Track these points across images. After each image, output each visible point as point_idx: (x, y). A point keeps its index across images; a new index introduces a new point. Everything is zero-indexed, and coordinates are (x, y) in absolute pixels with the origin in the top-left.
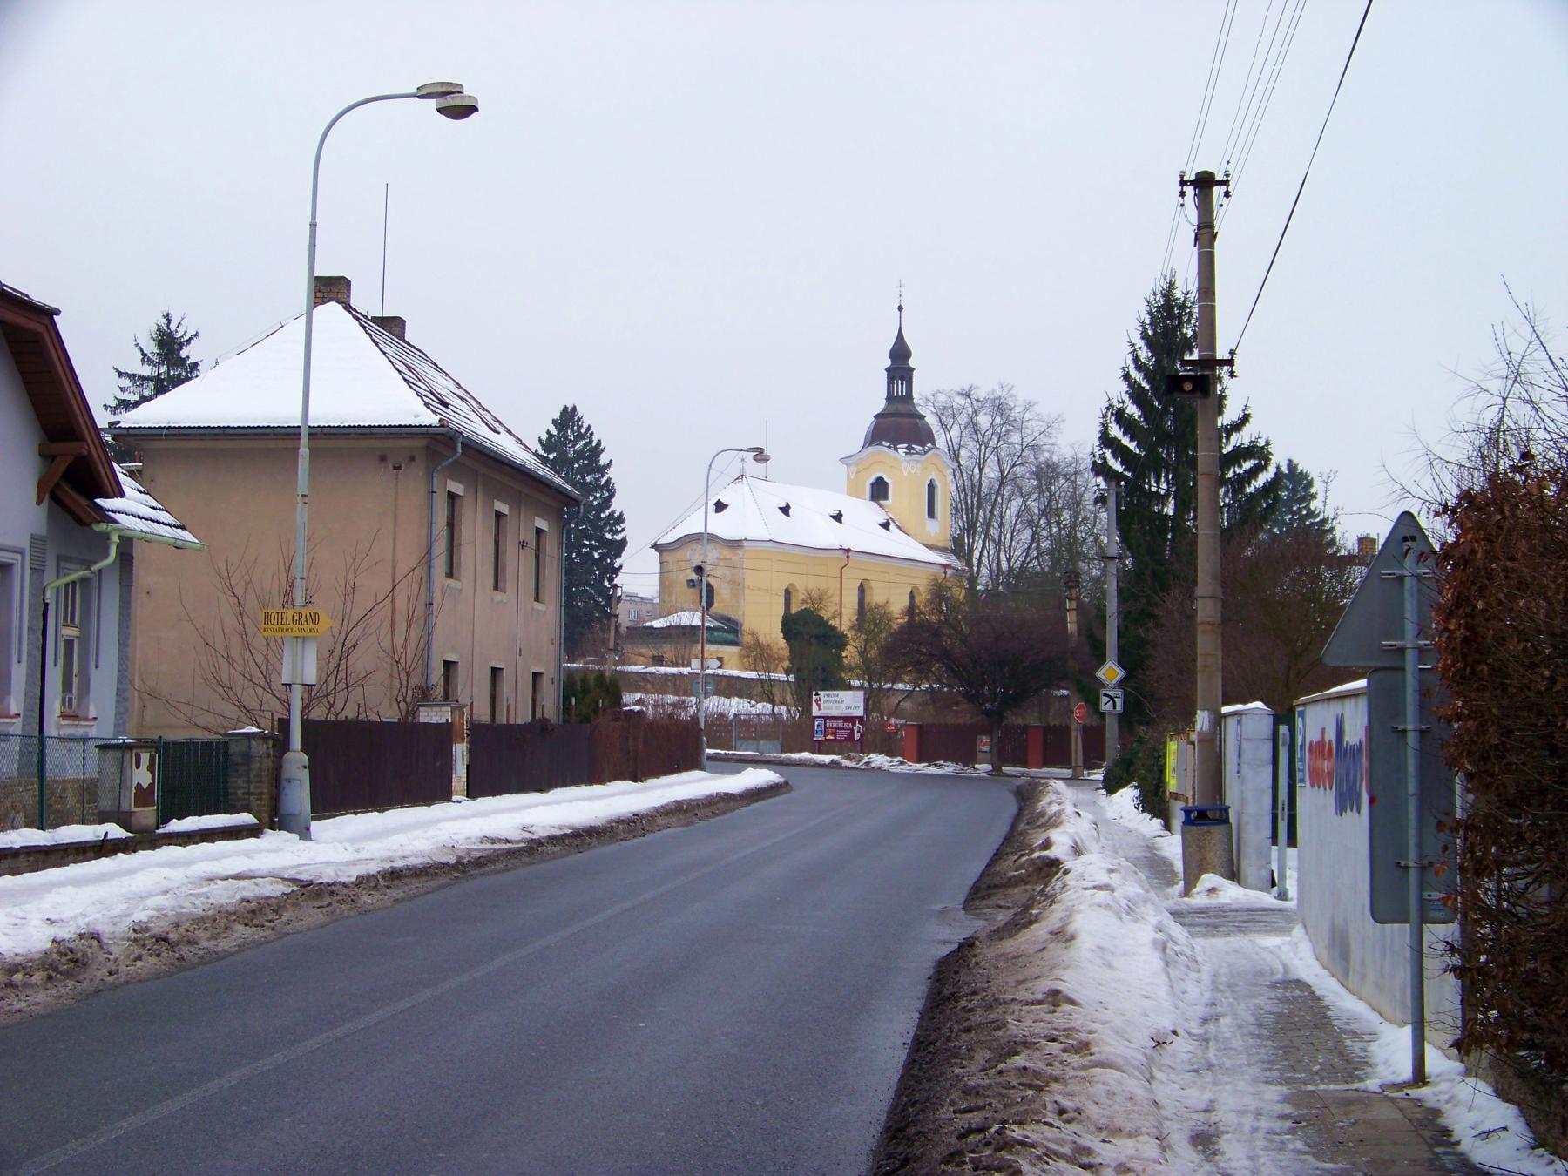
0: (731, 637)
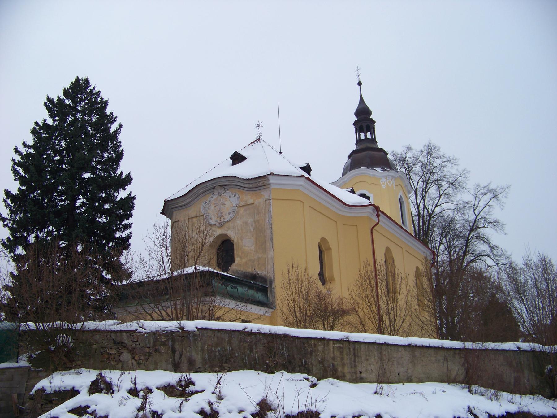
0: (259, 296)
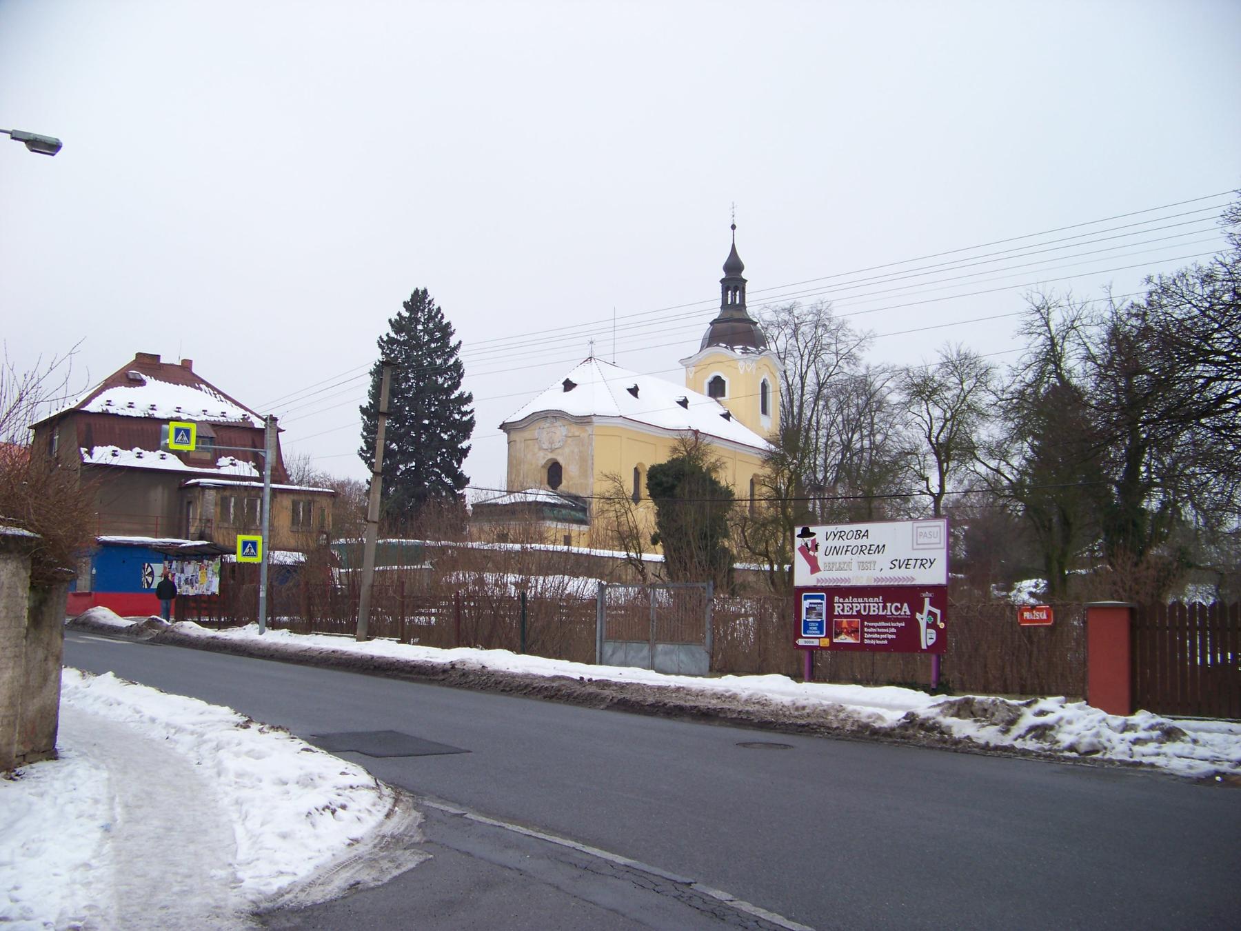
0: (580, 515)
